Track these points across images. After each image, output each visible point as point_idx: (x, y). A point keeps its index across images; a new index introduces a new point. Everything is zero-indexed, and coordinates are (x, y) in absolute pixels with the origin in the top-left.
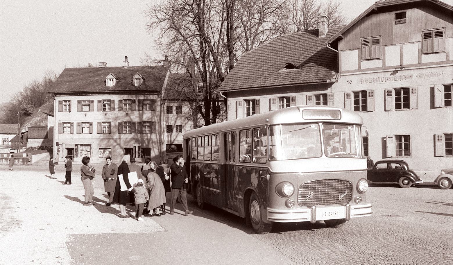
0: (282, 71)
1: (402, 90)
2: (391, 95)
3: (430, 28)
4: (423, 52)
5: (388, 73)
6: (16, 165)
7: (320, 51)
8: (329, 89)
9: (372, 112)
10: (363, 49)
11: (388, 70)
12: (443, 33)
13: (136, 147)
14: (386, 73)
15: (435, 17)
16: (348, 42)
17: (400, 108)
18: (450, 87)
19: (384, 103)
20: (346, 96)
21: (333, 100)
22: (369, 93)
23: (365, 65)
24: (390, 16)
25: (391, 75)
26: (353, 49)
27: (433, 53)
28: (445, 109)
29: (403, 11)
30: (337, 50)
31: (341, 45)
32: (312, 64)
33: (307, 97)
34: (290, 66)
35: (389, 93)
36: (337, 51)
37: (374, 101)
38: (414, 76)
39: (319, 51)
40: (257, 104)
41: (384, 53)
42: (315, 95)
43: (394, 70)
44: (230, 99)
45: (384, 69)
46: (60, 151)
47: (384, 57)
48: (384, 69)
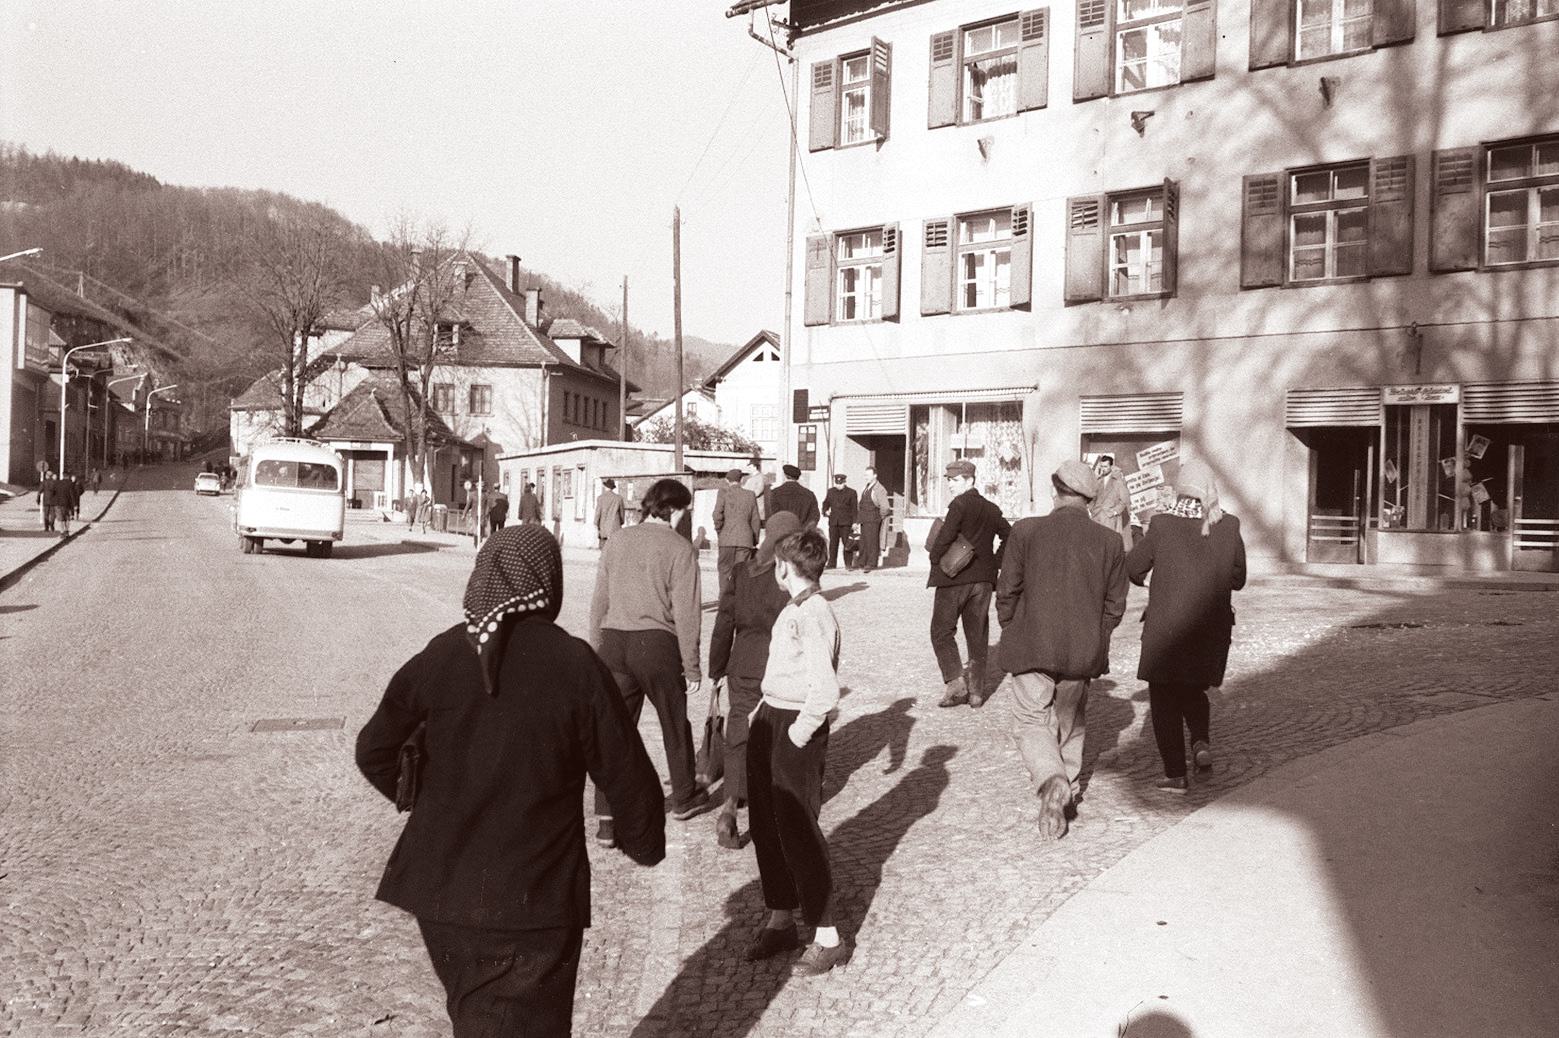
13: (1415, 417)
29: (760, 704)
46: (814, 460)
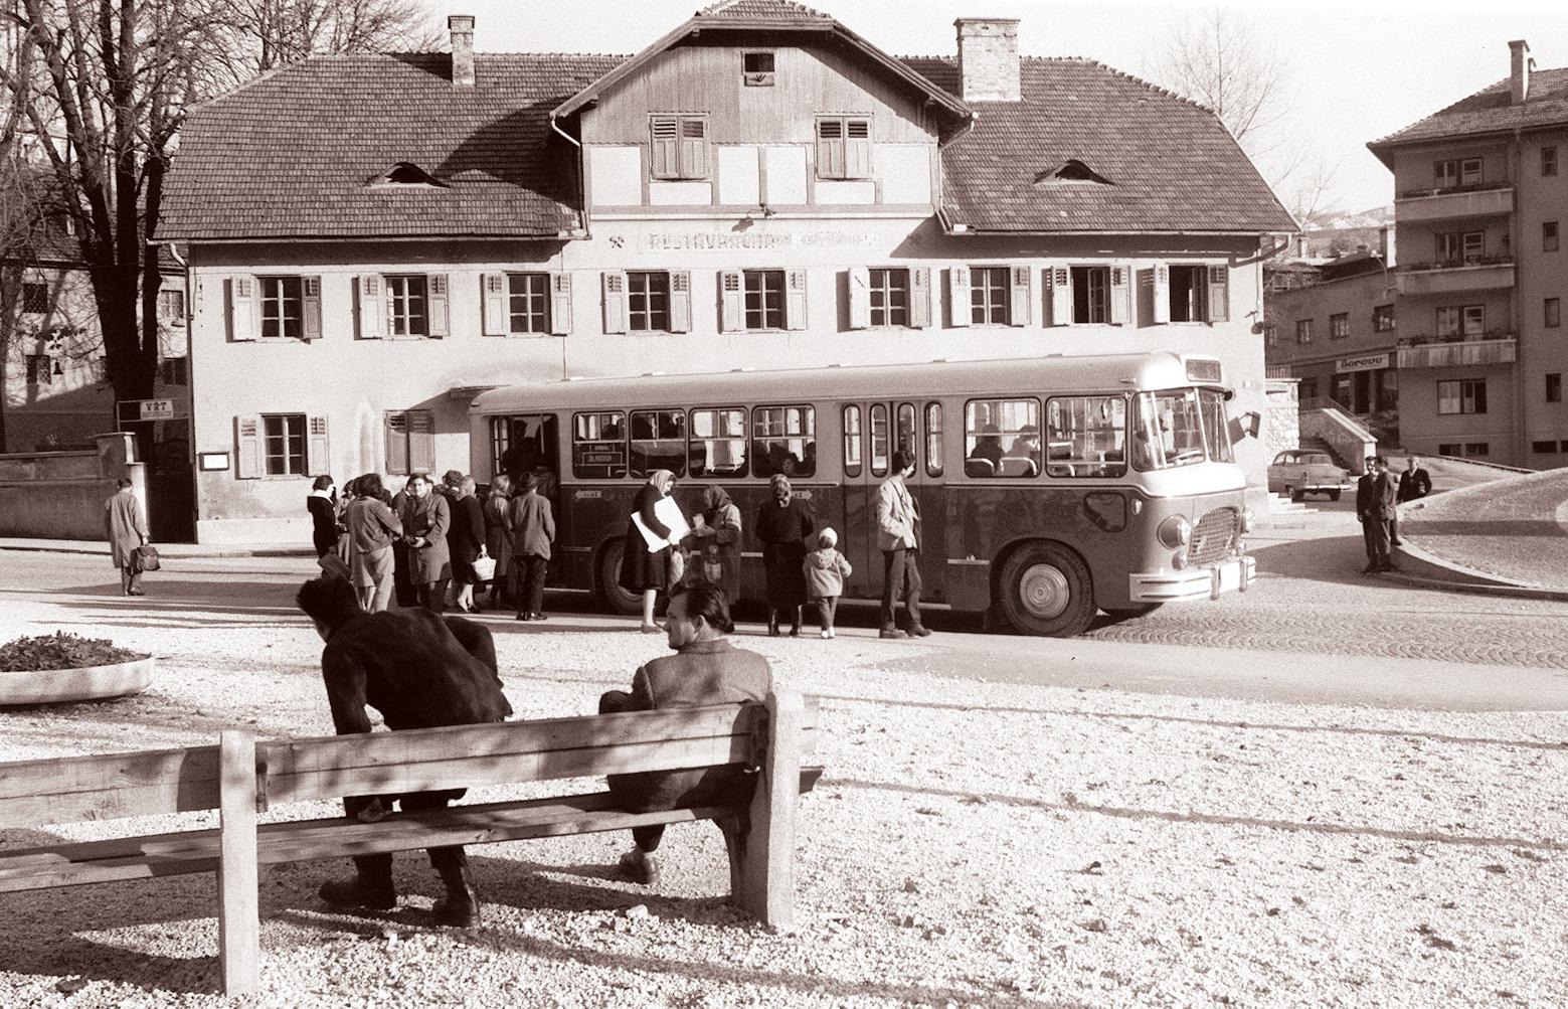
0: (380, 186)
1: (280, 282)
2: (736, 287)
3: (833, 113)
4: (817, 173)
5: (726, 223)
6: (1248, 414)
7: (481, 132)
8: (554, 258)
9: (684, 333)
10: (656, 146)
11: (727, 216)
12: (868, 127)
14: (721, 222)
15: (848, 81)
16: (613, 118)
17: (277, 334)
18: (525, 280)
19: (351, 316)
20: (606, 283)
21: (568, 295)
22: (1018, 272)
23: (663, 194)
24: (731, 60)
25: (735, 229)
26: (627, 144)
27: (844, 179)
28: (872, 333)
30: (579, 140)
31: (590, 126)
32: (476, 172)
33: (486, 281)
34: (407, 173)
35: (732, 283)
36: (578, 144)
37: (689, 302)
38: (796, 240)
39: (479, 132)
40: (308, 294)
41: (716, 168)
42: (260, 277)
43: (744, 216)
44: (199, 269)
45: (715, 210)
47: (716, 174)
48: (715, 210)
